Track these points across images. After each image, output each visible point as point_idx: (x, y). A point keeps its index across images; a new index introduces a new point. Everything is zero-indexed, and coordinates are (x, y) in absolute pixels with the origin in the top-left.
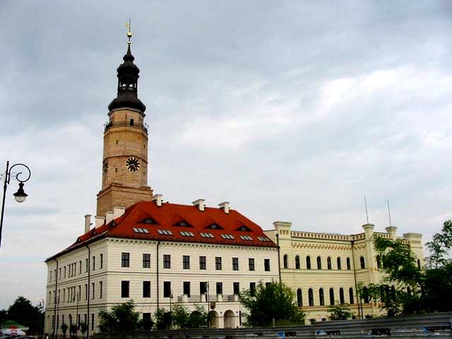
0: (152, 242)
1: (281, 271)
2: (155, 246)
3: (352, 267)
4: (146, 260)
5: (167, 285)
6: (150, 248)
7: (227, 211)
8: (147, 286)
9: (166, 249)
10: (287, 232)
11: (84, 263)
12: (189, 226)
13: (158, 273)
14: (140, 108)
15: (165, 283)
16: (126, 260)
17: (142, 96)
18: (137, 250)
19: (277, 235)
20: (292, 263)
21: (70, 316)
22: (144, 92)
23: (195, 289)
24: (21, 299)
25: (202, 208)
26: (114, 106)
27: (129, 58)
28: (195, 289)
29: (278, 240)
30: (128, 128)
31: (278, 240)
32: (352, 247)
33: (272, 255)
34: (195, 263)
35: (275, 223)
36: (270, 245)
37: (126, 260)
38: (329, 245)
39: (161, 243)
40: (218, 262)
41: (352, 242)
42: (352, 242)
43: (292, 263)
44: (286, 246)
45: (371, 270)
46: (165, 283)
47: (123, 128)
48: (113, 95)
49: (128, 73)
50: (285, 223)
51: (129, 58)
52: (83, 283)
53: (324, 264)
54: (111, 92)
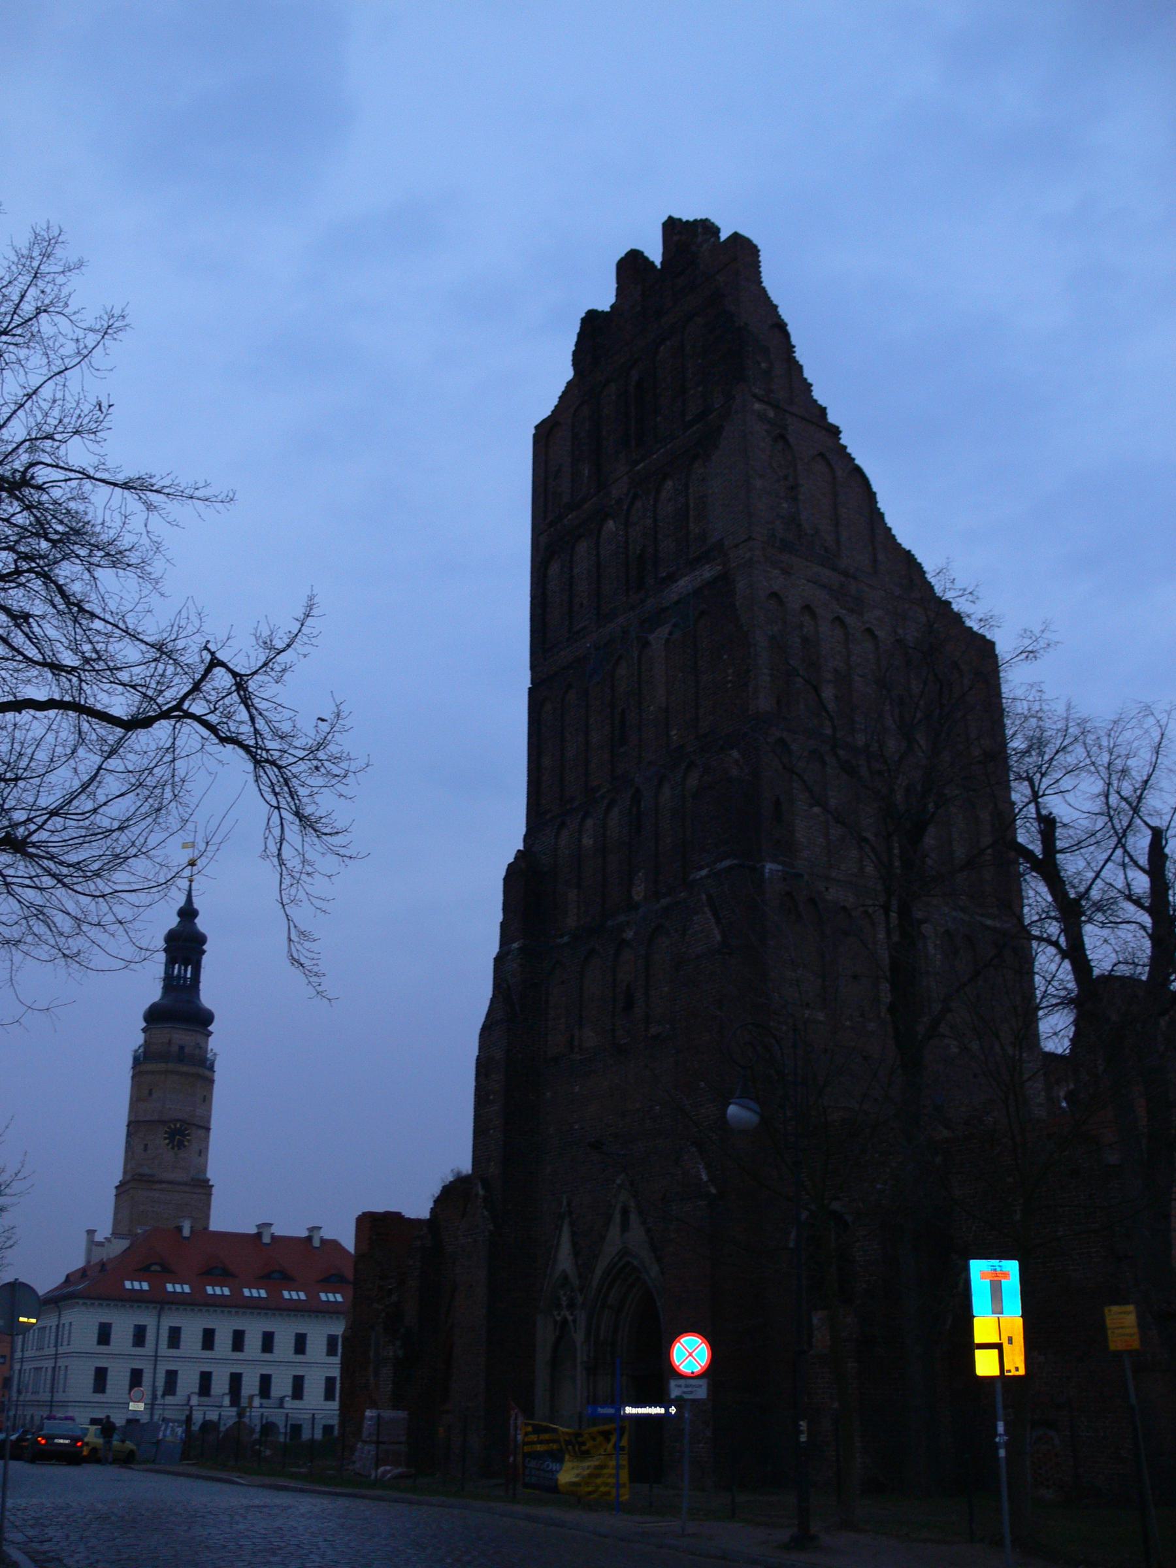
0: (151, 1306)
5: (172, 1376)
6: (148, 1319)
7: (316, 1243)
9: (170, 1320)
11: (54, 1328)
12: (222, 1274)
13: (156, 1356)
14: (203, 1019)
15: (334, 1400)
16: (104, 1335)
17: (208, 997)
21: (32, 1416)
22: (214, 988)
23: (220, 1385)
25: (266, 1239)
26: (154, 1016)
27: (188, 913)
28: (220, 1385)
30: (171, 1066)
34: (223, 1340)
37: (104, 1335)
38: (46, 1547)
39: (166, 1307)
40: (268, 1342)
47: (162, 1066)
48: (154, 993)
49: (185, 945)
51: (188, 913)
52: (51, 1364)
54: (148, 985)
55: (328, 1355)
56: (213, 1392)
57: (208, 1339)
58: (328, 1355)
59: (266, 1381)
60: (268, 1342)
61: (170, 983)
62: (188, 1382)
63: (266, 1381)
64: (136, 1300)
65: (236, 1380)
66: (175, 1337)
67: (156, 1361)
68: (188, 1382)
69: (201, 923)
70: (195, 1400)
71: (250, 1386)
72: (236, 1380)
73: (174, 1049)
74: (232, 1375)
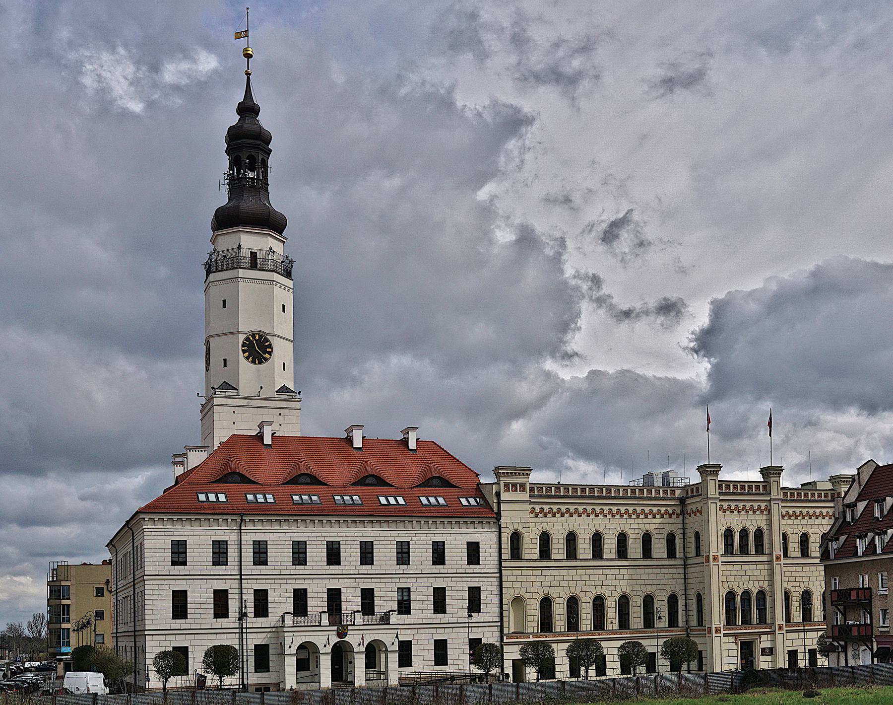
1: (504, 564)
2: (235, 527)
3: (679, 552)
4: (220, 553)
5: (261, 597)
6: (225, 532)
8: (221, 597)
9: (253, 533)
10: (523, 486)
13: (241, 575)
15: (226, 616)
17: (279, 199)
18: (200, 538)
19: (498, 494)
20: (531, 548)
23: (317, 603)
24: (665, 299)
26: (225, 220)
27: (248, 109)
28: (317, 603)
29: (499, 504)
31: (499, 504)
32: (682, 513)
33: (486, 539)
35: (497, 468)
36: (487, 511)
41: (682, 501)
42: (682, 501)
43: (531, 548)
44: (516, 514)
45: (710, 632)
46: (226, 616)
50: (515, 468)
51: (248, 109)
53: (794, 547)
55: (185, 592)
56: (310, 610)
57: (300, 554)
58: (185, 592)
59: (368, 596)
60: (367, 554)
61: (236, 186)
62: (281, 602)
63: (368, 596)
64: (214, 512)
65: (334, 596)
66: (261, 554)
67: (241, 579)
68: (281, 602)
69: (265, 120)
70: (289, 620)
71: (351, 603)
72: (334, 596)
73: (245, 254)
74: (266, 615)
